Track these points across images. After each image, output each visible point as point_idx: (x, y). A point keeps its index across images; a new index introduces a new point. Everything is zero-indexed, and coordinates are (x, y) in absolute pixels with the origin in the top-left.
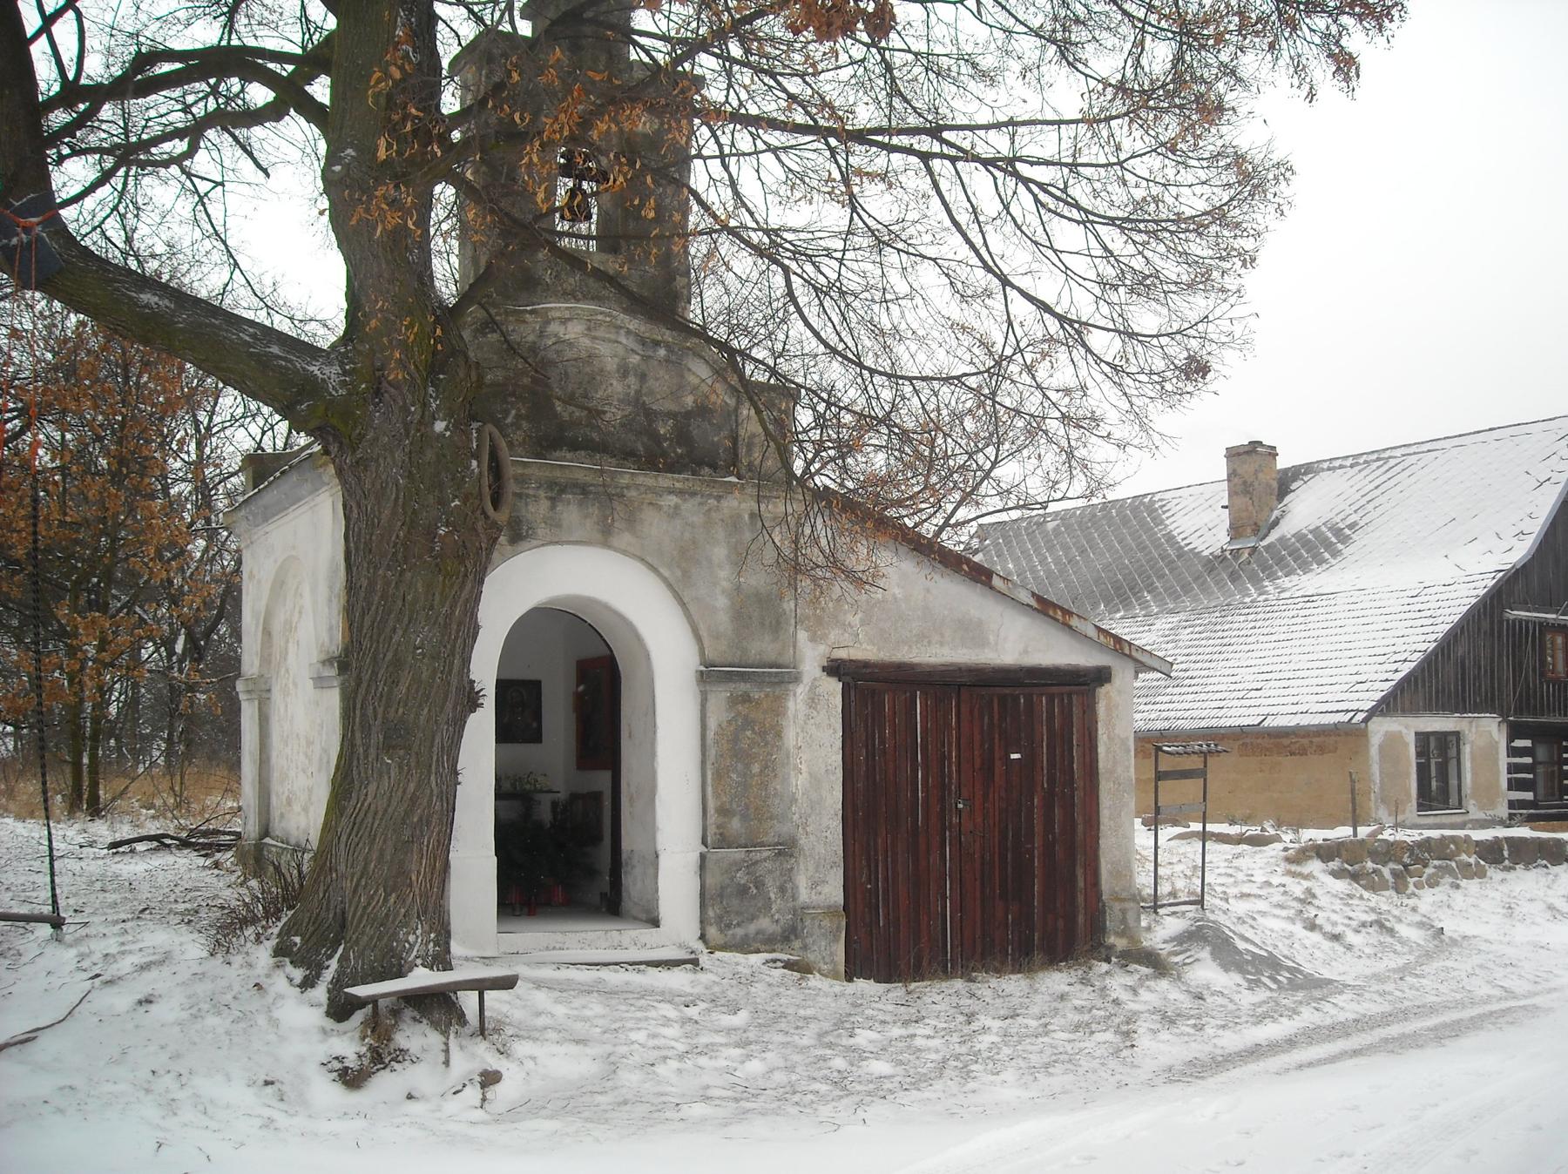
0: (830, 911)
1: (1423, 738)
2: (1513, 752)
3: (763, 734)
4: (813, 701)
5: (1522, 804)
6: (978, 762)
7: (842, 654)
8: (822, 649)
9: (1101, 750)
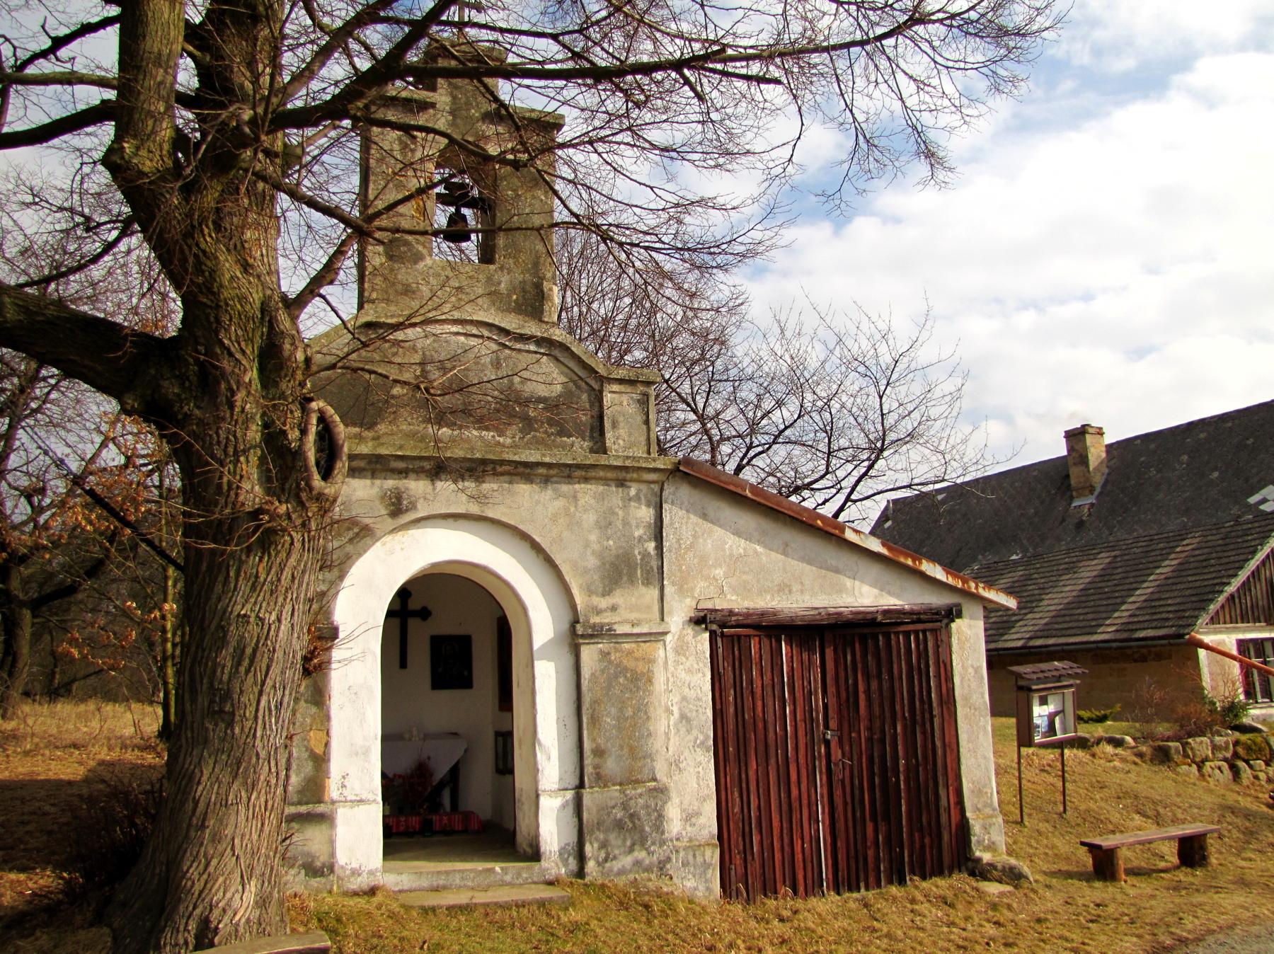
9: (957, 680)
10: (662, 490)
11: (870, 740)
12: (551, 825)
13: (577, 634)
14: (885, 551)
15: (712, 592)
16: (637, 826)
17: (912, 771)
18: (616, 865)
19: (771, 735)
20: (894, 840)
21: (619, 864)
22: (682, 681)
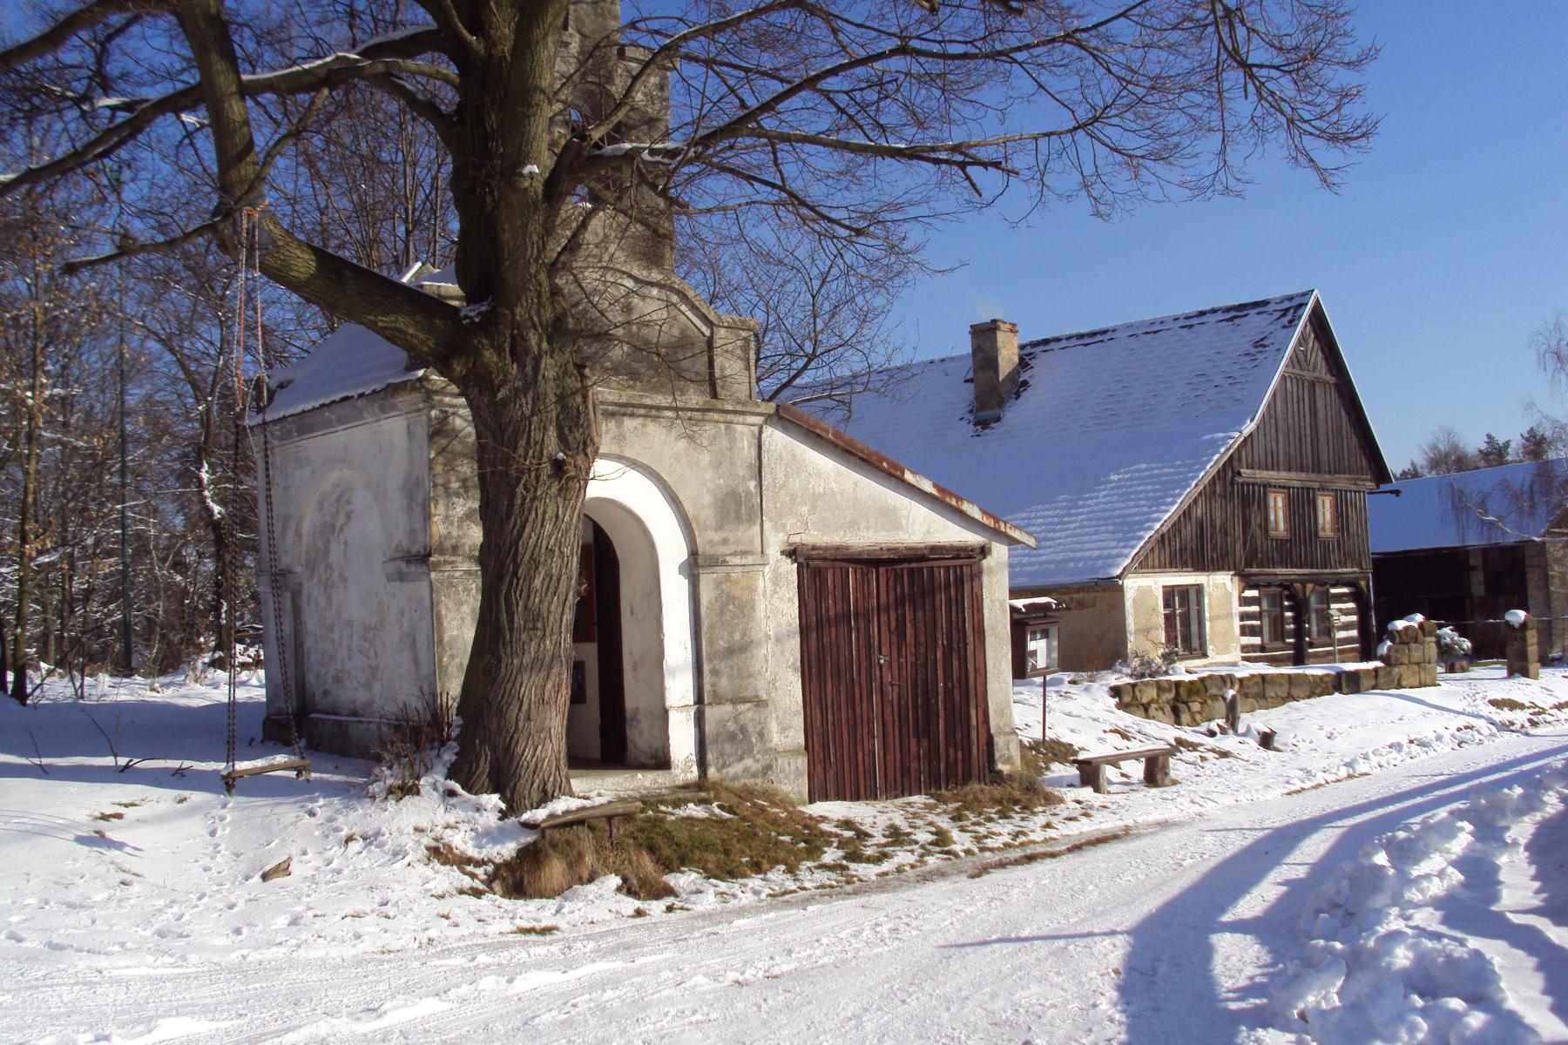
0: (795, 752)
1: (1169, 593)
2: (1245, 601)
3: (741, 607)
4: (776, 581)
5: (1253, 648)
6: (893, 624)
7: (796, 539)
8: (782, 536)
9: (986, 611)
10: (760, 432)
11: (915, 664)
12: (682, 741)
13: (694, 566)
14: (935, 492)
15: (799, 527)
16: (740, 739)
17: (948, 693)
18: (732, 771)
19: (842, 659)
20: (933, 754)
21: (734, 771)
22: (776, 605)
